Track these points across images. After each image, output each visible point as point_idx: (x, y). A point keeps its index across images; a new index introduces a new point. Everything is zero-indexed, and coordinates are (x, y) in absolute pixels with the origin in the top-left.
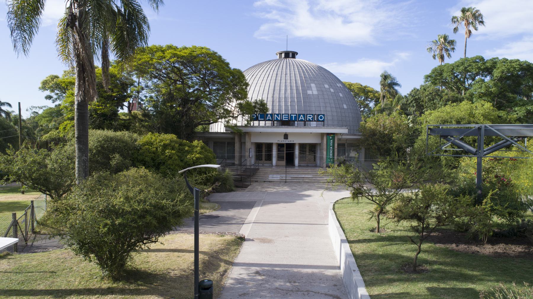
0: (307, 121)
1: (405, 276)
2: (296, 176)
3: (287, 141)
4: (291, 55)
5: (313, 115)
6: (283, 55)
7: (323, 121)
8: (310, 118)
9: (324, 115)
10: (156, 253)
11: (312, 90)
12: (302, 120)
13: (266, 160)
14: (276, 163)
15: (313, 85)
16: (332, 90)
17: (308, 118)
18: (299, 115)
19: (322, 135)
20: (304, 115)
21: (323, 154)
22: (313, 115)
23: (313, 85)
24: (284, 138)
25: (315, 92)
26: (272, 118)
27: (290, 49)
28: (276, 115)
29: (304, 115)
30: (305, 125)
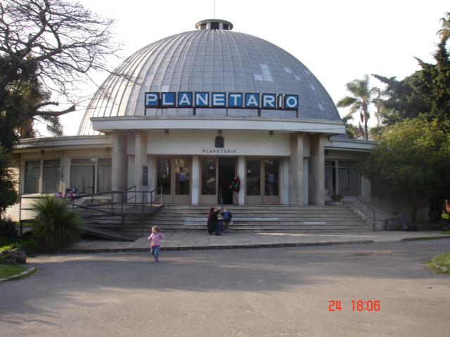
0: (264, 108)
1: (50, 144)
2: (271, 219)
3: (221, 152)
4: (221, 25)
5: (274, 95)
6: (208, 27)
7: (296, 109)
8: (270, 102)
9: (297, 96)
10: (196, 245)
11: (261, 73)
12: (252, 107)
13: (177, 193)
14: (200, 199)
15: (264, 67)
16: (298, 78)
17: (265, 101)
18: (248, 95)
19: (293, 137)
20: (257, 95)
21: (294, 178)
22: (274, 95)
23: (264, 67)
24: (217, 145)
25: (269, 79)
26: (191, 102)
27: (218, 17)
28: (198, 96)
29: (257, 95)
30: (259, 115)
